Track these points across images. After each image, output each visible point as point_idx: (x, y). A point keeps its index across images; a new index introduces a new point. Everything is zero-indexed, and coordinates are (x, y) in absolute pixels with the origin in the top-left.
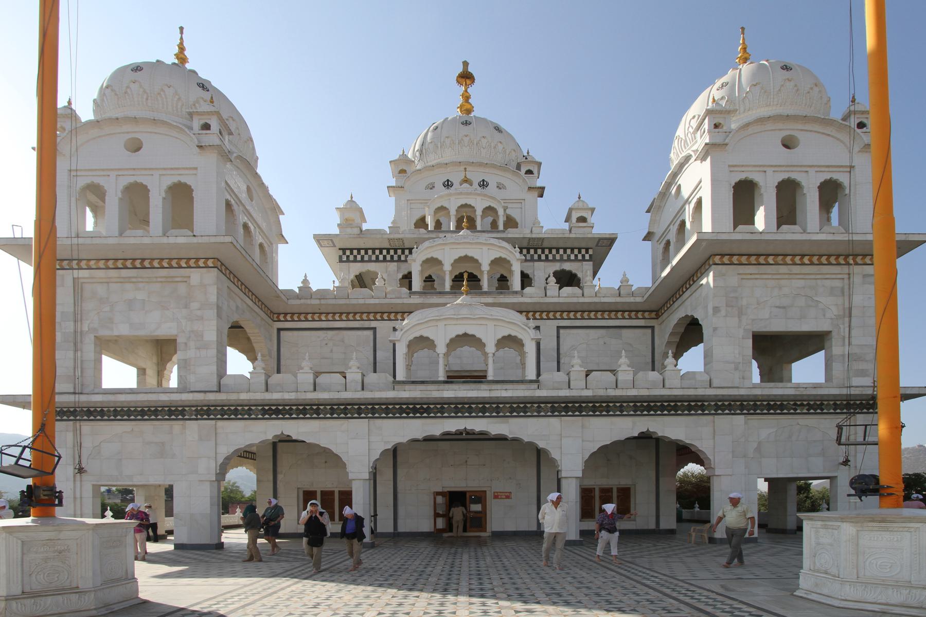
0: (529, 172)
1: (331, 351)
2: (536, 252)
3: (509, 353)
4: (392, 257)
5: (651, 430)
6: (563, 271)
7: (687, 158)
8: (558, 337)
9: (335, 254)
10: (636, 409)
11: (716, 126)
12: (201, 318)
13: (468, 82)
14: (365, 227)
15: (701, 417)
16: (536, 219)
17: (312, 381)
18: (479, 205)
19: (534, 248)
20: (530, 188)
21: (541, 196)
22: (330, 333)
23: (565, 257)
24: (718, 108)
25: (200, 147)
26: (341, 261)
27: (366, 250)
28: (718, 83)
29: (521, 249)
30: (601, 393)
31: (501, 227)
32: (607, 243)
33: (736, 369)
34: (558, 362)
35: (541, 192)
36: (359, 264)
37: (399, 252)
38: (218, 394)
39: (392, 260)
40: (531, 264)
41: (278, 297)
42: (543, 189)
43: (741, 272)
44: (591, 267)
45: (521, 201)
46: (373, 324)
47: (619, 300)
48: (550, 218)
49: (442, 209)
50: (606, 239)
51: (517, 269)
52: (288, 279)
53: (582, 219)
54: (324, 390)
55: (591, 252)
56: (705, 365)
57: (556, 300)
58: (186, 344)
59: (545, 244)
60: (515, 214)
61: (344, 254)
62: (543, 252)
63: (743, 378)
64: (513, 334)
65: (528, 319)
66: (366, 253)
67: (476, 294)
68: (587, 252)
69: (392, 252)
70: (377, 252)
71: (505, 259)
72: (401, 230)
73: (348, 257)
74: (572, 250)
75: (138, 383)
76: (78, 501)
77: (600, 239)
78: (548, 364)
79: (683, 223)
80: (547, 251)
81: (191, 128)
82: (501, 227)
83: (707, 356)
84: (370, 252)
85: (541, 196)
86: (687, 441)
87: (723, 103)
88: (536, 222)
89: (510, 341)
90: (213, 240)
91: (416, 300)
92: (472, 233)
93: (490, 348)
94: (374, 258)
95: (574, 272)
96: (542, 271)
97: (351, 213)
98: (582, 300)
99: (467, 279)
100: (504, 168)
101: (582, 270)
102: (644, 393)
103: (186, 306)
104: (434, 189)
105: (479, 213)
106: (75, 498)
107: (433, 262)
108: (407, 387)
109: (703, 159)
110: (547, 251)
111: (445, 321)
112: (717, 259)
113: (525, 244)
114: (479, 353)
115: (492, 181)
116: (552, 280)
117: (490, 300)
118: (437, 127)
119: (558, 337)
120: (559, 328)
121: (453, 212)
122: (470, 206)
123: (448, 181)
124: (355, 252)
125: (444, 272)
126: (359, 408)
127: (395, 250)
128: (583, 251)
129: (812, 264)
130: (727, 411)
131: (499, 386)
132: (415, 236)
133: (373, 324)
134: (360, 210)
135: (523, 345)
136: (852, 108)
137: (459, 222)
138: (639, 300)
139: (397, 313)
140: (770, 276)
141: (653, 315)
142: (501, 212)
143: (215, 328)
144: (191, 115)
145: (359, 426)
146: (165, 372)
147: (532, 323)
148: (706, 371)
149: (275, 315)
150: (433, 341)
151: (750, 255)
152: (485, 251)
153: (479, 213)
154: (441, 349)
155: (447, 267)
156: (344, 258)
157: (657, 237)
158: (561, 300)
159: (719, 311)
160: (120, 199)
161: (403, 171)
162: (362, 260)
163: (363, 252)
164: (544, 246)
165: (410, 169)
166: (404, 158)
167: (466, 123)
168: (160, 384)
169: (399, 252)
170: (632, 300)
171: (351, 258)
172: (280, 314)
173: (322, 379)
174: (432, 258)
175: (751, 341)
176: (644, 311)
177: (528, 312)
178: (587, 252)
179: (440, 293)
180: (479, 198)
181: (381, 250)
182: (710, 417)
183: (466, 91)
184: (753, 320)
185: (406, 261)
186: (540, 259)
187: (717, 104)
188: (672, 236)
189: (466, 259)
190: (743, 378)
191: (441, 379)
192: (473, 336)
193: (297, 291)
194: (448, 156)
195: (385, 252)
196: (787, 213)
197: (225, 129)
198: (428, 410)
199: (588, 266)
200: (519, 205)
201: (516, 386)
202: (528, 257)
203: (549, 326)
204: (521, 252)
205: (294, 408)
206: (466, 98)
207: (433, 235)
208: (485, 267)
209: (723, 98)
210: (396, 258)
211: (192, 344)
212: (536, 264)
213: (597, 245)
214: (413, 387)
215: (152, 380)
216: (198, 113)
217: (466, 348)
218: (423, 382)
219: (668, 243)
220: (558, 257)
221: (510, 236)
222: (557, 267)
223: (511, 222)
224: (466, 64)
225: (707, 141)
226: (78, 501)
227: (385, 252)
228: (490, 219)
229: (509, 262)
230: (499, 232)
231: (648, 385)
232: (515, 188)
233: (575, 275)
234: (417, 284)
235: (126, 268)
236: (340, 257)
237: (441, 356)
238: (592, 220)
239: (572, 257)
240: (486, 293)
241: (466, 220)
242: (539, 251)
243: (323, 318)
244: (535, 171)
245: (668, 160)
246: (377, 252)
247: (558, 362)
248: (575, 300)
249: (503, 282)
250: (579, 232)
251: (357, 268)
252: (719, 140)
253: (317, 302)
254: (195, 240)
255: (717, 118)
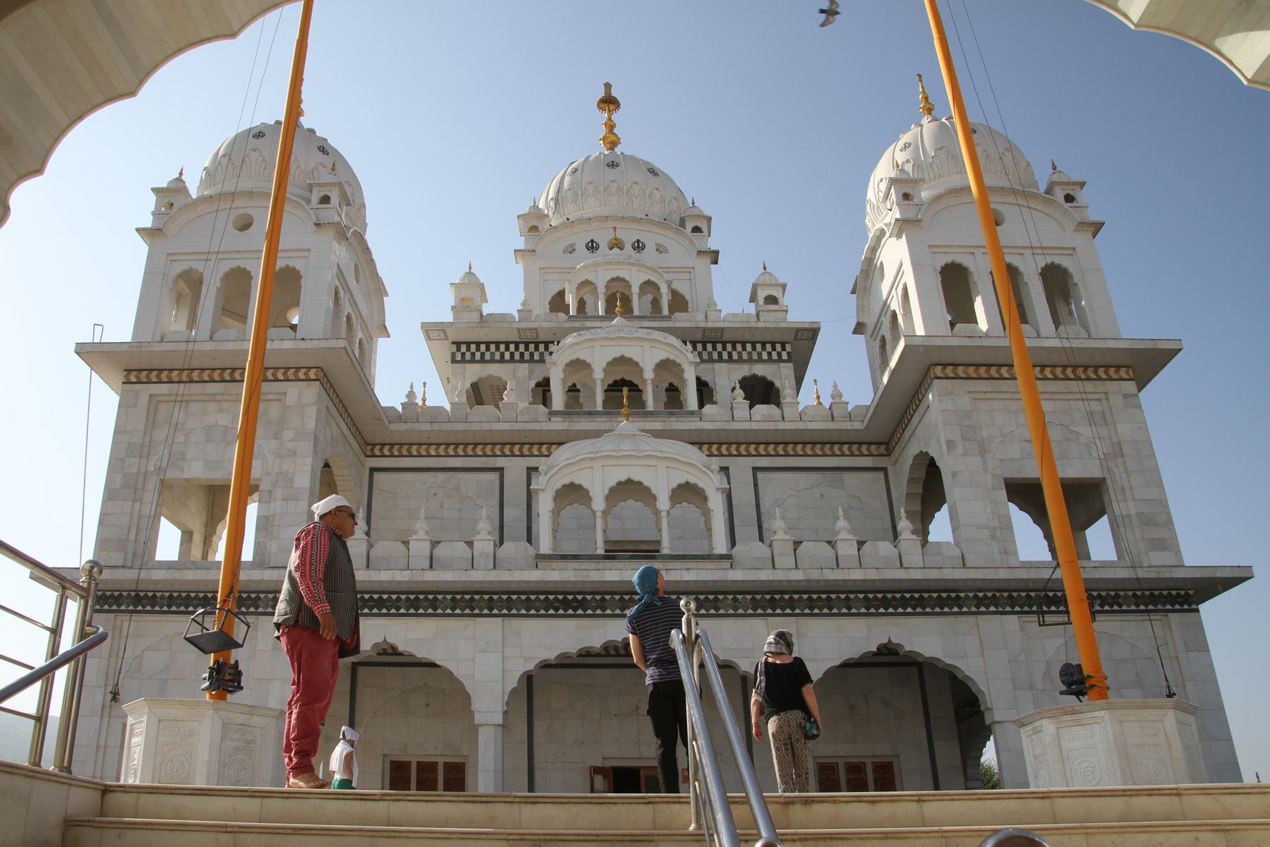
0: (697, 229)
1: (442, 507)
2: (714, 349)
3: (688, 510)
4: (522, 355)
5: (894, 641)
6: (754, 377)
7: (882, 232)
8: (756, 485)
9: (446, 349)
10: (868, 603)
11: (906, 196)
12: (294, 454)
13: (612, 107)
14: (487, 309)
15: (960, 618)
16: (711, 298)
17: (428, 554)
18: (636, 279)
19: (713, 342)
20: (699, 253)
21: (716, 262)
22: (441, 476)
23: (755, 357)
24: (903, 176)
25: (318, 225)
26: (454, 361)
27: (488, 344)
28: (900, 144)
29: (694, 344)
30: (815, 575)
31: (666, 312)
32: (809, 335)
33: (993, 537)
34: (760, 528)
35: (714, 257)
36: (478, 366)
37: (532, 347)
38: (757, 465)
39: (522, 360)
40: (709, 366)
41: (380, 419)
42: (717, 253)
43: (971, 389)
44: (792, 372)
45: (689, 270)
46: (500, 462)
47: (831, 426)
48: (728, 299)
49: (586, 283)
50: (806, 329)
51: (690, 376)
52: (390, 389)
53: (772, 300)
54: (445, 568)
55: (788, 348)
56: (954, 530)
57: (746, 426)
58: (270, 492)
59: (726, 337)
60: (683, 289)
61: (459, 350)
62: (724, 349)
63: (1006, 553)
64: (693, 480)
65: (711, 455)
66: (488, 349)
67: (638, 414)
68: (784, 349)
69: (522, 347)
70: (502, 347)
71: (674, 362)
72: (535, 314)
73: (463, 354)
74: (763, 344)
75: (180, 555)
76: (102, 750)
77: (798, 330)
78: (746, 530)
79: (894, 315)
80: (729, 347)
81: (309, 201)
82: (666, 312)
83: (953, 517)
84: (493, 347)
85: (716, 262)
86: (948, 661)
87: (909, 168)
88: (711, 304)
89: (687, 493)
90: (324, 344)
91: (558, 424)
92: (629, 336)
93: (663, 503)
94: (497, 356)
95: (769, 378)
96: (726, 377)
97: (470, 290)
98: (781, 426)
99: (623, 390)
100: (664, 223)
101: (781, 375)
102: (873, 575)
103: (277, 436)
104: (575, 254)
105: (635, 290)
106: (98, 746)
107: (578, 365)
108: (555, 564)
109: (899, 236)
110: (729, 347)
111: (603, 459)
112: (938, 370)
113: (699, 336)
114: (648, 511)
115: (650, 241)
116: (740, 393)
117: (657, 425)
118: (576, 170)
119: (756, 485)
120: (373, 470)
121: (601, 289)
122: (623, 280)
123: (592, 241)
124: (473, 347)
125: (594, 381)
126: (491, 599)
127: (529, 346)
128: (778, 347)
129: (1056, 378)
130: (992, 609)
131: (678, 564)
132: (553, 325)
133: (500, 462)
134: (481, 287)
135: (706, 498)
136: (1056, 178)
137: (610, 301)
138: (857, 425)
139: (532, 444)
140: (1009, 396)
141: (882, 449)
142: (664, 289)
143: (309, 468)
144: (311, 187)
145: (489, 628)
146: (214, 539)
147: (716, 463)
148: (957, 544)
149: (370, 447)
150: (587, 492)
151: (978, 366)
152: (649, 350)
153: (635, 290)
154: (599, 504)
155: (598, 374)
156: (459, 358)
157: (870, 329)
158: (754, 426)
159: (955, 447)
160: (219, 289)
161: (534, 229)
162: (482, 360)
163: (483, 347)
164: (724, 339)
165: (544, 227)
166: (536, 213)
167: (613, 165)
168: (205, 556)
169: (532, 347)
170: (848, 426)
171: (468, 356)
172: (374, 445)
173: (440, 552)
174: (578, 359)
175: (1004, 492)
176: (870, 444)
177: (710, 444)
178: (784, 349)
179: (590, 413)
180: (634, 270)
181: (507, 344)
182: (972, 618)
183: (610, 119)
184: (1001, 460)
185: (542, 361)
186: (720, 359)
187: (902, 171)
188: (886, 330)
189: (622, 361)
190: (1006, 553)
191: (601, 551)
192: (640, 483)
193: (400, 409)
194: (592, 208)
195: (512, 347)
196: (1016, 309)
197: (346, 201)
198: (583, 604)
199: (787, 370)
200: (687, 276)
201: (701, 564)
202: (705, 356)
203: (741, 467)
204: (695, 348)
205: (403, 597)
206: (611, 127)
207: (577, 324)
208: (649, 374)
209: (908, 161)
210: (527, 356)
211: (279, 493)
212: (717, 366)
213: (795, 338)
214: (561, 564)
215: (196, 553)
216: (319, 185)
217: (630, 503)
218: (575, 557)
219: (883, 340)
220: (745, 356)
221: (678, 325)
222: (744, 371)
223: (679, 303)
224: (608, 86)
225: (898, 216)
226: (102, 750)
227: (512, 347)
228: (650, 297)
229: (679, 365)
230: (663, 318)
231: (883, 562)
232: (679, 252)
233: (771, 384)
234: (558, 398)
235: (212, 381)
236: (453, 355)
237: (599, 514)
238: (785, 301)
239: (765, 356)
240: (651, 413)
241: (618, 301)
242: (719, 347)
243: (433, 453)
244: (705, 228)
245: (865, 229)
246: (502, 347)
247: (760, 528)
248: (771, 426)
249: (673, 394)
250: (769, 320)
251: (474, 372)
252: (911, 215)
253: (427, 427)
254: (302, 345)
255: (904, 189)
